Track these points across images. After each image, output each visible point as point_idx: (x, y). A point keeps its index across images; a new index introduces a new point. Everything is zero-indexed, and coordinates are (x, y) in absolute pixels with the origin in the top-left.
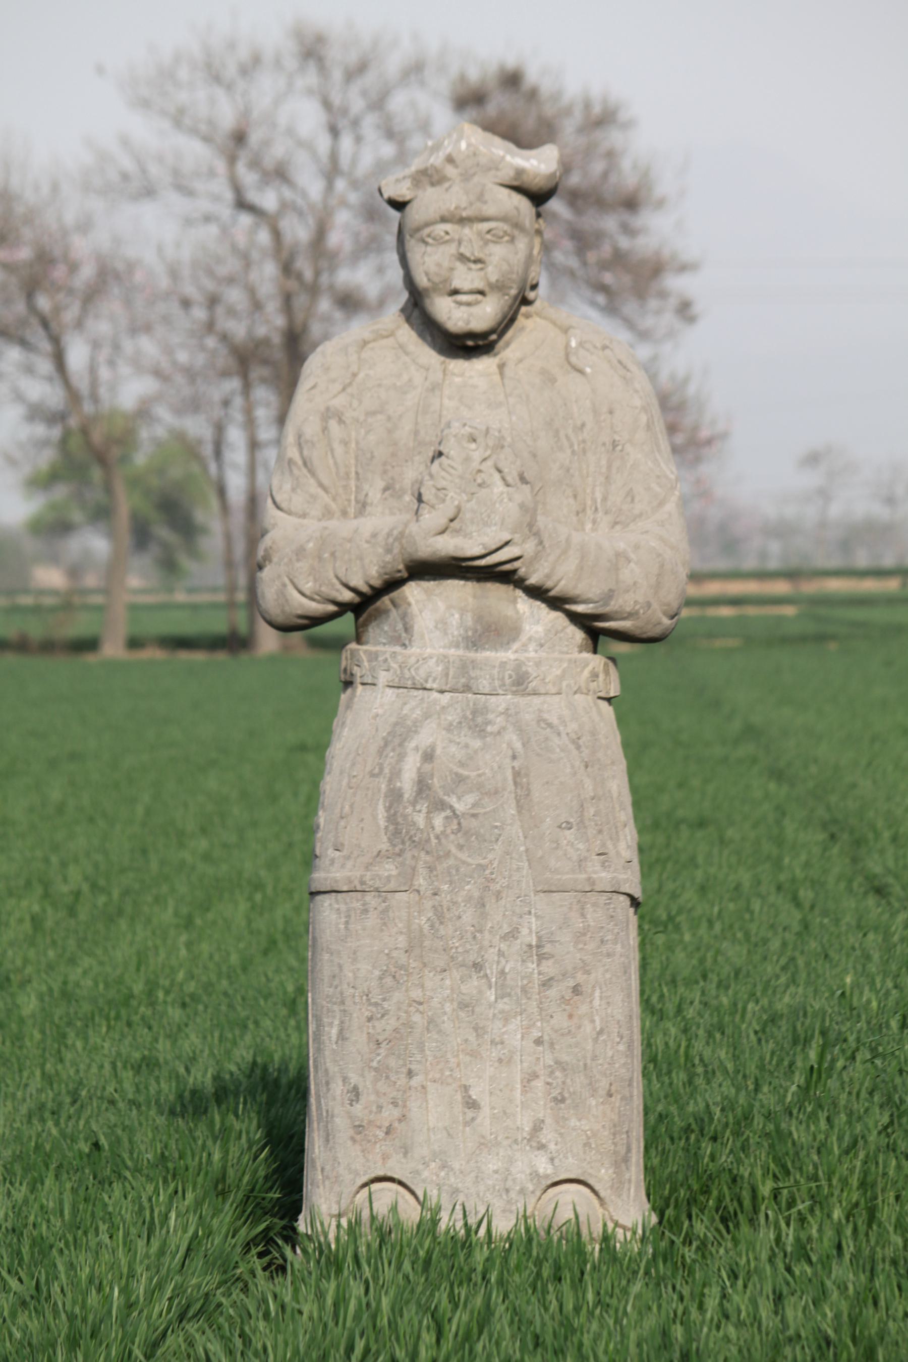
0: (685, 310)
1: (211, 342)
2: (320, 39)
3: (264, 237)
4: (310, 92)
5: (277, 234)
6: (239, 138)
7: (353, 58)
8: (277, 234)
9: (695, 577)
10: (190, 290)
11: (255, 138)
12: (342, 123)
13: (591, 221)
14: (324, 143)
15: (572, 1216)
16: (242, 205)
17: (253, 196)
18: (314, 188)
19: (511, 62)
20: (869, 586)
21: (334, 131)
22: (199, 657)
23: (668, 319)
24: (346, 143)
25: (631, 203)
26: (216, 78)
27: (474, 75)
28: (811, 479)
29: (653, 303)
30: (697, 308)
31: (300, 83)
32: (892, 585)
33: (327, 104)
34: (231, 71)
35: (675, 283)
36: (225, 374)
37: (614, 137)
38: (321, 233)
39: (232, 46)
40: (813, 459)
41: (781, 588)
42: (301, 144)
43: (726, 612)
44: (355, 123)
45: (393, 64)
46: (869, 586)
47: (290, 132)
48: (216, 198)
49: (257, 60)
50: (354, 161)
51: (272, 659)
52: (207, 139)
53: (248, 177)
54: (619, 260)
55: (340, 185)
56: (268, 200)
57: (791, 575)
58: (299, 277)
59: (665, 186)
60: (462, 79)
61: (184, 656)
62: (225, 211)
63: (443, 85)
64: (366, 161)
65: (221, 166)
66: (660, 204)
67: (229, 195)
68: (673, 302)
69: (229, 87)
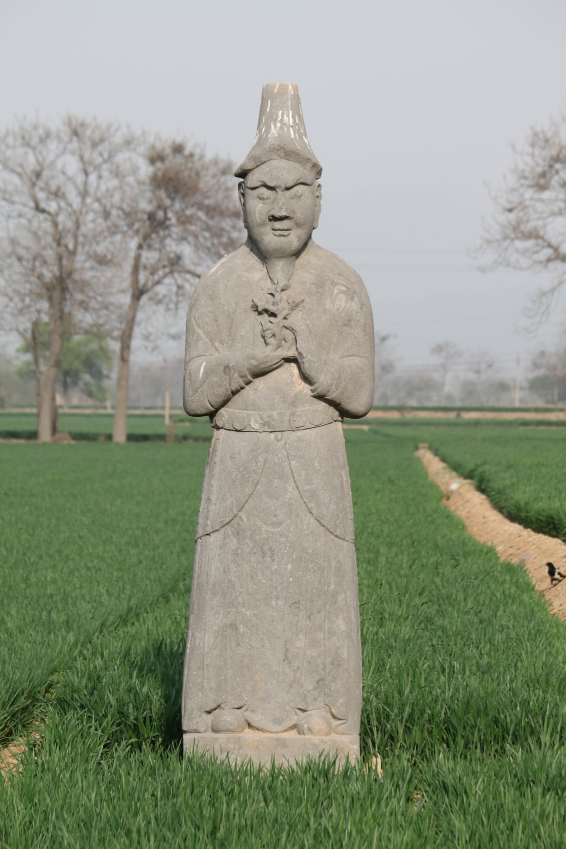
1: (33, 279)
3: (47, 226)
4: (73, 153)
5: (55, 224)
6: (38, 175)
7: (97, 136)
8: (55, 224)
10: (21, 252)
11: (46, 174)
12: (90, 169)
14: (80, 178)
16: (38, 209)
17: (43, 205)
19: (179, 140)
20: (440, 415)
21: (86, 173)
22: (22, 442)
24: (93, 178)
26: (27, 144)
28: (437, 360)
33: (82, 158)
34: (35, 141)
36: (40, 296)
38: (78, 225)
39: (36, 127)
40: (439, 349)
42: (69, 179)
44: (97, 168)
45: (118, 139)
46: (440, 415)
47: (63, 173)
48: (24, 205)
49: (48, 135)
50: (98, 188)
51: (44, 444)
52: (20, 175)
53: (41, 195)
55: (89, 200)
56: (52, 206)
57: (400, 409)
58: (66, 246)
61: (15, 441)
62: (30, 212)
63: (142, 149)
65: (26, 189)
67: (32, 204)
69: (34, 149)
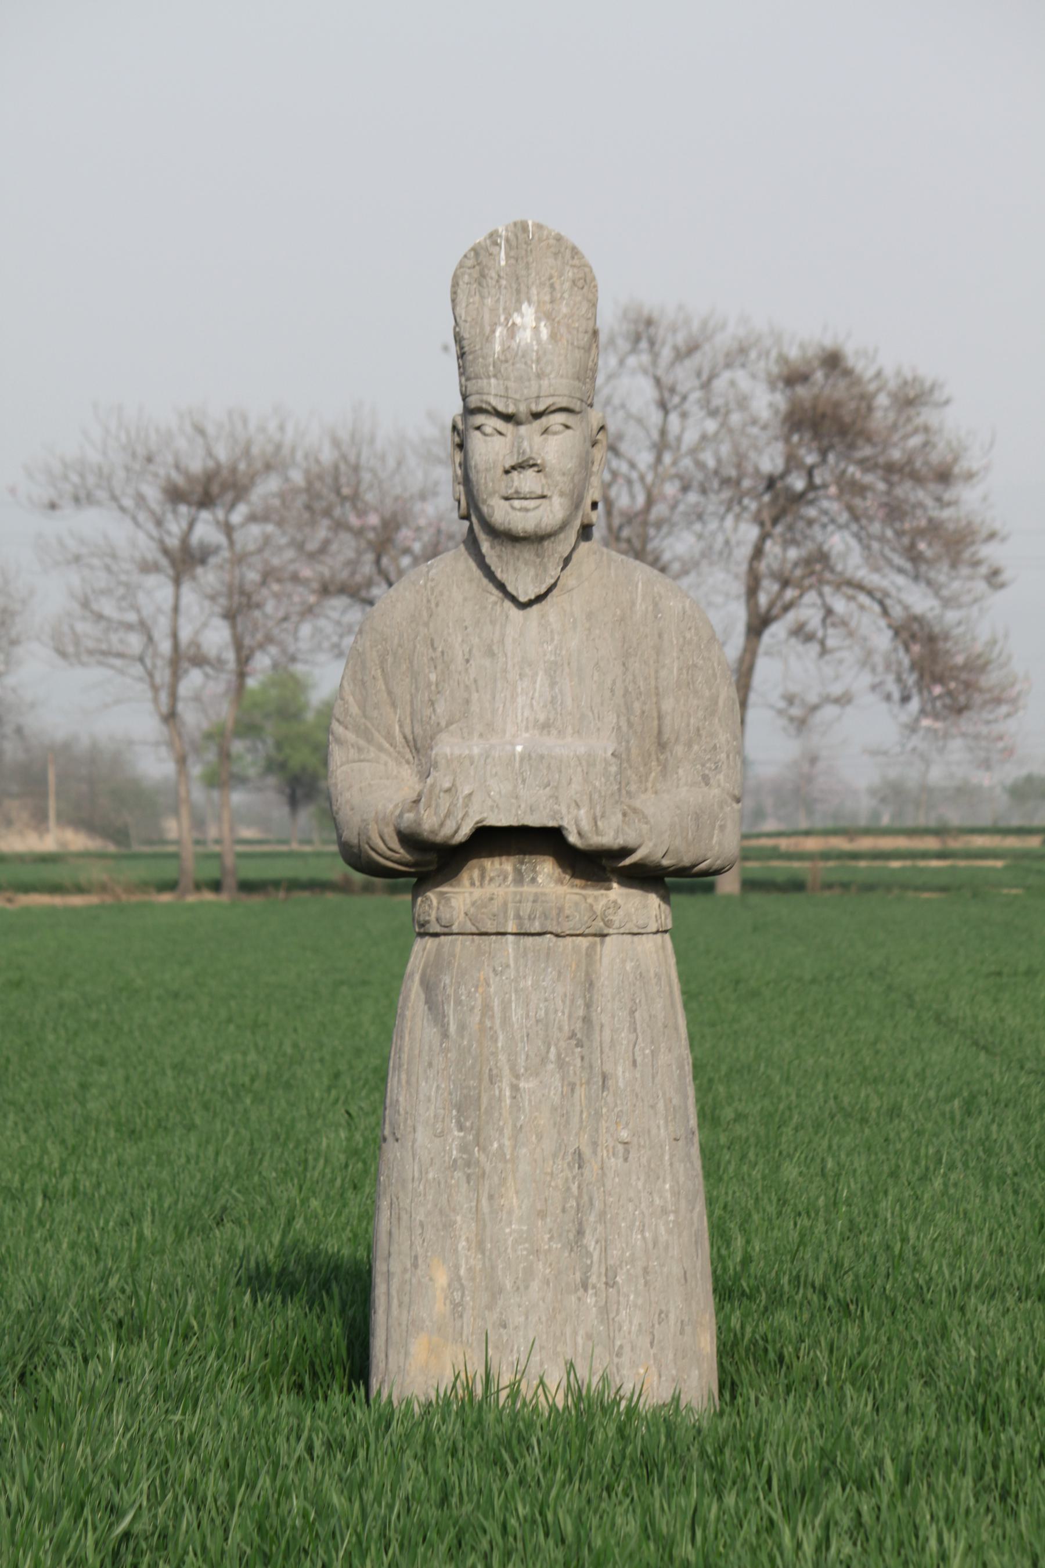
0: (994, 578)
2: (649, 322)
7: (680, 339)
9: (745, 837)
13: (905, 490)
15: (481, 1371)
18: (645, 459)
21: (663, 406)
23: (981, 586)
24: (674, 418)
25: (944, 476)
27: (793, 353)
29: (965, 571)
30: (1005, 577)
31: (632, 361)
32: (1033, 842)
33: (658, 381)
35: (988, 551)
37: (927, 416)
41: (931, 843)
43: (935, 863)
45: (724, 341)
51: (729, 898)
54: (934, 529)
59: (971, 461)
60: (782, 359)
64: (690, 437)
66: (970, 476)
68: (983, 570)
